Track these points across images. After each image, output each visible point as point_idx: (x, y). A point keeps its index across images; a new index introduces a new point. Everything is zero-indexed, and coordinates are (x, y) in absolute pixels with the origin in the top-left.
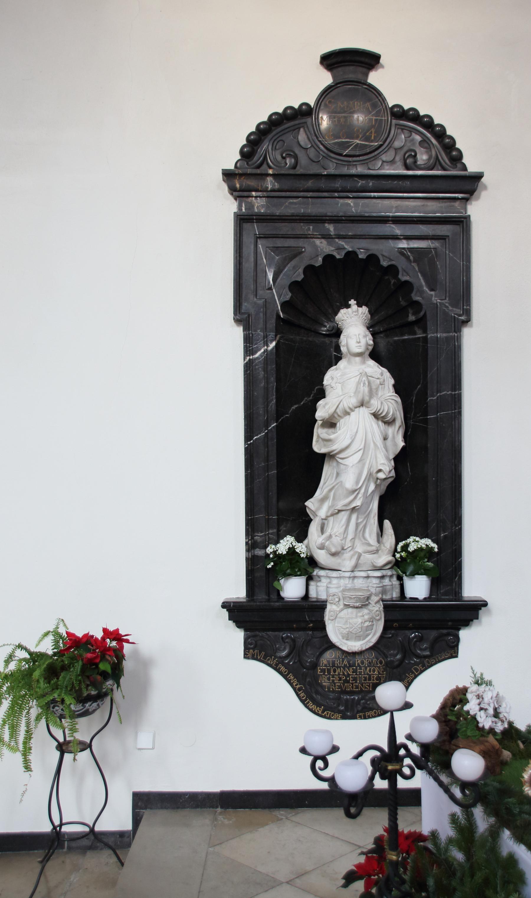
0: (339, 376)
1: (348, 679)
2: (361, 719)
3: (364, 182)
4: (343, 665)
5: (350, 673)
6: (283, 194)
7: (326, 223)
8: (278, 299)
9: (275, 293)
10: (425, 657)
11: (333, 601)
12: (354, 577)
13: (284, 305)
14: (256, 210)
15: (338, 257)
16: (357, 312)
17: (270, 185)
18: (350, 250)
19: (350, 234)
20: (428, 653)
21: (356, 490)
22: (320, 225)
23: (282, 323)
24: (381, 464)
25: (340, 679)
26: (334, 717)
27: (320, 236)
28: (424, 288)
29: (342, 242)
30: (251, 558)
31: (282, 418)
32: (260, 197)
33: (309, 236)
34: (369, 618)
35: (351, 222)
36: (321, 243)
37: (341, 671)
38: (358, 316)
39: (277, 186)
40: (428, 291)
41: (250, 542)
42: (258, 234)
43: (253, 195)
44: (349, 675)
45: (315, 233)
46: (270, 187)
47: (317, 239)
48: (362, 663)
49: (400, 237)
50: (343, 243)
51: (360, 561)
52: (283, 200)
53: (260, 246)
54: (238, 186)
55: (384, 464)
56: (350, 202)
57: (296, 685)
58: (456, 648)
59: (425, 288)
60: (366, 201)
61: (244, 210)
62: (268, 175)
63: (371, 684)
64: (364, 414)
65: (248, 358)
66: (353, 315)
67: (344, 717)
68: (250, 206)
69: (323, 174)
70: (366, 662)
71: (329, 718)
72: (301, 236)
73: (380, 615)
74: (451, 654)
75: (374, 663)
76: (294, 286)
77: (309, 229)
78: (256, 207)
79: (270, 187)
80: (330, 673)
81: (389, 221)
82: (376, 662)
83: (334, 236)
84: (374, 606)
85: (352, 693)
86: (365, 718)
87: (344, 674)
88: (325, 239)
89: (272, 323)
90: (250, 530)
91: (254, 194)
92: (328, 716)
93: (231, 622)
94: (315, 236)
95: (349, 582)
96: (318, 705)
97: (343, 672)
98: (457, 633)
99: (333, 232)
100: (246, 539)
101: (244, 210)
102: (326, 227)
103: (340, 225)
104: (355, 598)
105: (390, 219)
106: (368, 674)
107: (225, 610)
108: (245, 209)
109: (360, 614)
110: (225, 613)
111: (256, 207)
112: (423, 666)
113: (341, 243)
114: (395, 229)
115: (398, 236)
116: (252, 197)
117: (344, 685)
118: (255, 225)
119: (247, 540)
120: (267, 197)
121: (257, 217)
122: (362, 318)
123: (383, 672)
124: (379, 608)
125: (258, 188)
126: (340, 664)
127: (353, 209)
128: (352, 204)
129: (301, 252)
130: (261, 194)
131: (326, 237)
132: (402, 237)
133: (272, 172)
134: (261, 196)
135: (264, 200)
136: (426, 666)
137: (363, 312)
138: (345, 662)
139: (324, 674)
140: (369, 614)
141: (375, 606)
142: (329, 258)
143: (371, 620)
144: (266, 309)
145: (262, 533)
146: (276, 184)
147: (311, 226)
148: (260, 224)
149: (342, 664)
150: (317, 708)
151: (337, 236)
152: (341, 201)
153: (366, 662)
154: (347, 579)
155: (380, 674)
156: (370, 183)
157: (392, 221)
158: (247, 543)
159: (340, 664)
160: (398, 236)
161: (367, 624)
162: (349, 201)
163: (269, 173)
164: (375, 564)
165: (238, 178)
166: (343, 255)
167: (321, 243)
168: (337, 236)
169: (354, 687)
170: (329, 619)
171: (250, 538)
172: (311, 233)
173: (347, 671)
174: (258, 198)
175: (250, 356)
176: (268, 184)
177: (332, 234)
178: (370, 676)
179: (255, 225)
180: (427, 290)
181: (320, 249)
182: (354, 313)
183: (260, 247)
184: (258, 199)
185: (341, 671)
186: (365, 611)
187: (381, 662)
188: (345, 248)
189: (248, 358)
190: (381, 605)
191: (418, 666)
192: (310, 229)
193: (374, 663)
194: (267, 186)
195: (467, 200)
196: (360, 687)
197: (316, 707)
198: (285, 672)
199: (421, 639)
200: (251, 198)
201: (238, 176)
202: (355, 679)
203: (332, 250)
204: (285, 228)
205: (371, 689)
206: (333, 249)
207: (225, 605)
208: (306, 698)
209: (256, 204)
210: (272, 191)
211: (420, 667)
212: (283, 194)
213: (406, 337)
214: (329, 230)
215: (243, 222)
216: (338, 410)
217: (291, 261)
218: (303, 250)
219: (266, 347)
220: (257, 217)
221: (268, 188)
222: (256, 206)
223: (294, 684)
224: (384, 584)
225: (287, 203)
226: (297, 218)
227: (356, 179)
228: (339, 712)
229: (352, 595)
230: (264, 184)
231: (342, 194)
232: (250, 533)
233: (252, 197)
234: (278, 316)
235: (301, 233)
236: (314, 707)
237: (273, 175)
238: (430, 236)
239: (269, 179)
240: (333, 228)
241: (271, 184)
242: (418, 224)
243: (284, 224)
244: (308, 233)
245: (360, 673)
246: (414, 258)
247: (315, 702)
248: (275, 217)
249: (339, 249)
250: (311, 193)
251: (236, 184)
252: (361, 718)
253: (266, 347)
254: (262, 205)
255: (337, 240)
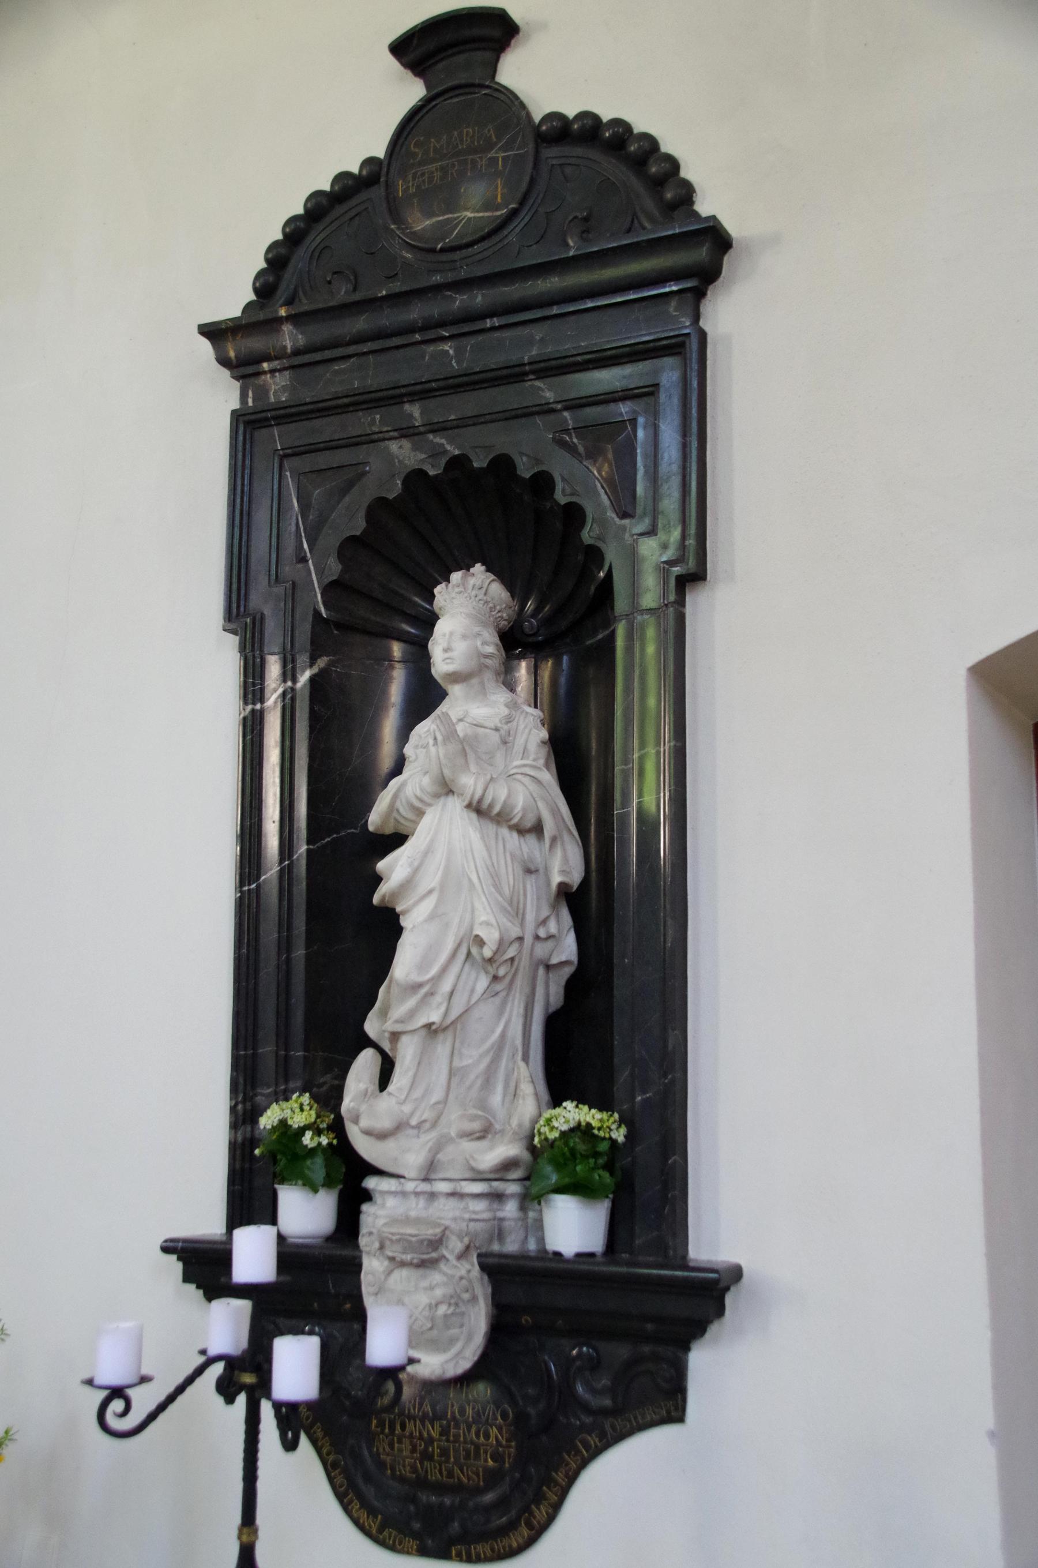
0: (425, 733)
1: (430, 1449)
2: (461, 1560)
3: (465, 297)
4: (420, 1414)
5: (434, 1435)
6: (318, 356)
7: (405, 402)
8: (317, 579)
9: (312, 568)
10: (604, 1412)
11: (369, 1246)
12: (432, 1196)
13: (331, 589)
14: (272, 400)
15: (432, 472)
16: (461, 586)
17: (288, 341)
18: (457, 452)
19: (453, 417)
20: (607, 1402)
21: (420, 985)
22: (394, 409)
23: (335, 632)
24: (481, 924)
25: (414, 1450)
26: (404, 1547)
27: (395, 434)
28: (608, 514)
29: (441, 438)
30: (243, 1144)
31: (335, 836)
32: (279, 371)
33: (376, 437)
34: (444, 1296)
35: (452, 391)
36: (401, 447)
37: (415, 1427)
38: (466, 595)
39: (301, 340)
40: (617, 519)
41: (240, 1107)
42: (282, 449)
43: (263, 368)
44: (431, 1441)
45: (385, 429)
46: (289, 345)
47: (393, 441)
48: (462, 1411)
49: (553, 406)
50: (443, 441)
51: (440, 1156)
52: (320, 369)
53: (288, 474)
54: (232, 354)
55: (487, 924)
56: (448, 348)
57: (328, 1454)
58: (679, 1396)
59: (611, 514)
60: (481, 338)
61: (250, 403)
62: (280, 320)
63: (481, 1469)
64: (454, 806)
65: (250, 707)
66: (454, 593)
67: (424, 1552)
68: (261, 393)
69: (380, 295)
70: (469, 1411)
71: (392, 1548)
72: (359, 439)
73: (470, 1291)
74: (668, 1412)
75: (489, 1415)
76: (350, 547)
77: (373, 422)
78: (272, 393)
79: (289, 345)
80: (394, 1430)
81: (526, 374)
82: (494, 1414)
83: (422, 429)
84: (456, 1267)
85: (440, 1488)
86: (469, 1560)
87: (421, 1437)
88: (407, 438)
89: (304, 630)
90: (241, 1080)
91: (265, 366)
92: (391, 1542)
93: (191, 1287)
94: (387, 435)
95: (417, 1204)
96: (372, 1512)
97: (420, 1433)
98: (681, 1355)
99: (419, 420)
100: (231, 1099)
101: (250, 403)
102: (406, 410)
103: (432, 403)
104: (399, 1241)
105: (527, 368)
106: (472, 1443)
107: (174, 1257)
108: (253, 402)
109: (425, 1283)
110: (174, 1266)
111: (272, 393)
112: (602, 1435)
113: (439, 440)
114: (543, 390)
115: (551, 406)
116: (265, 373)
117: (421, 1463)
118: (276, 431)
119: (233, 1102)
120: (292, 367)
121: (273, 413)
122: (477, 599)
123: (508, 1440)
124: (469, 1271)
125: (268, 351)
126: (414, 1409)
127: (454, 361)
128: (451, 352)
129: (364, 474)
130: (279, 364)
131: (407, 432)
132: (559, 406)
133: (285, 312)
134: (278, 367)
135: (288, 377)
136: (609, 1436)
137: (477, 584)
138: (428, 1408)
139: (382, 1432)
140: (445, 1284)
141: (459, 1265)
142: (416, 477)
143: (453, 1300)
144: (293, 604)
145: (268, 1088)
146: (300, 337)
147: (377, 414)
148: (282, 428)
149: (419, 1411)
150: (368, 1517)
151: (428, 427)
152: (431, 348)
153: (469, 1411)
154: (412, 1197)
155: (501, 1446)
156: (477, 297)
157: (533, 372)
158: (233, 1110)
159: (414, 1409)
160: (551, 406)
161: (442, 1310)
162: (448, 347)
163: (280, 314)
164: (473, 1164)
165: (231, 339)
166: (443, 465)
167: (401, 447)
168: (428, 427)
169: (445, 1473)
170: (369, 1293)
171: (240, 1099)
172: (377, 430)
173: (428, 1431)
174: (277, 374)
175: (254, 704)
176: (286, 341)
177: (417, 424)
178: (477, 1448)
179: (276, 431)
180: (614, 516)
181: (399, 461)
182: (457, 590)
183: (287, 476)
184: (276, 377)
185: (415, 1427)
186: (436, 1277)
187: (504, 1416)
188: (445, 452)
189: (250, 707)
190: (473, 1265)
191: (590, 1435)
192: (374, 421)
193: (489, 1415)
194: (284, 343)
195: (699, 294)
196: (458, 1475)
197: (366, 1516)
198: (308, 1418)
199: (594, 1365)
200: (263, 377)
201: (289, 351)
202: (444, 1452)
203: (421, 460)
204: (328, 428)
205: (482, 1483)
206: (423, 456)
207: (167, 1248)
208: (347, 1490)
209: (273, 387)
210: (297, 352)
211: (593, 1440)
212: (318, 356)
213: (600, 636)
214: (411, 416)
215: (254, 429)
216: (398, 804)
217: (344, 496)
218: (368, 468)
219: (289, 684)
220: (273, 413)
221: (285, 347)
222: (273, 391)
223: (325, 1451)
224: (500, 1214)
225: (328, 375)
226: (346, 400)
227: (449, 293)
228: (416, 1535)
229: (392, 1234)
230: (278, 340)
231: (431, 335)
232: (241, 1087)
233: (265, 373)
234: (317, 613)
235: (359, 433)
236: (363, 1516)
237: (290, 318)
238: (618, 392)
239: (287, 328)
240: (420, 411)
241: (290, 339)
242: (588, 369)
243: (325, 420)
244: (371, 430)
245: (457, 1437)
246: (586, 448)
247: (365, 1504)
248: (305, 408)
249: (436, 453)
250: (369, 344)
251: (228, 352)
252: (460, 1558)
253: (289, 684)
254: (283, 386)
255: (431, 436)
